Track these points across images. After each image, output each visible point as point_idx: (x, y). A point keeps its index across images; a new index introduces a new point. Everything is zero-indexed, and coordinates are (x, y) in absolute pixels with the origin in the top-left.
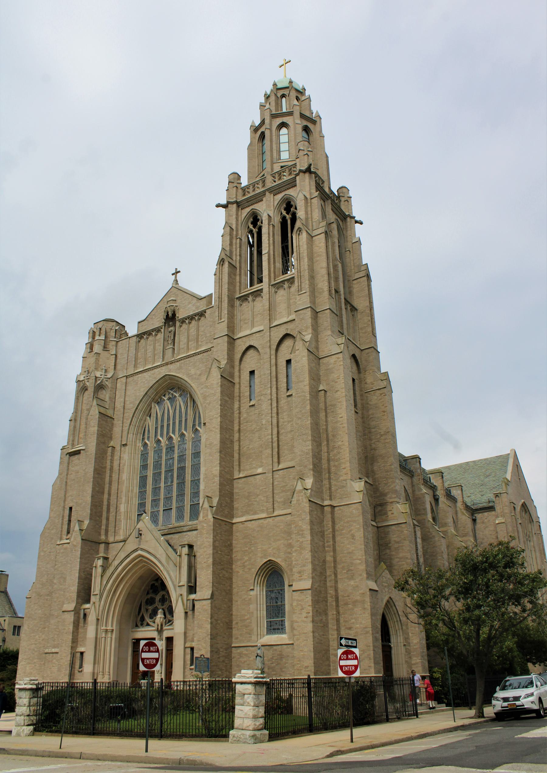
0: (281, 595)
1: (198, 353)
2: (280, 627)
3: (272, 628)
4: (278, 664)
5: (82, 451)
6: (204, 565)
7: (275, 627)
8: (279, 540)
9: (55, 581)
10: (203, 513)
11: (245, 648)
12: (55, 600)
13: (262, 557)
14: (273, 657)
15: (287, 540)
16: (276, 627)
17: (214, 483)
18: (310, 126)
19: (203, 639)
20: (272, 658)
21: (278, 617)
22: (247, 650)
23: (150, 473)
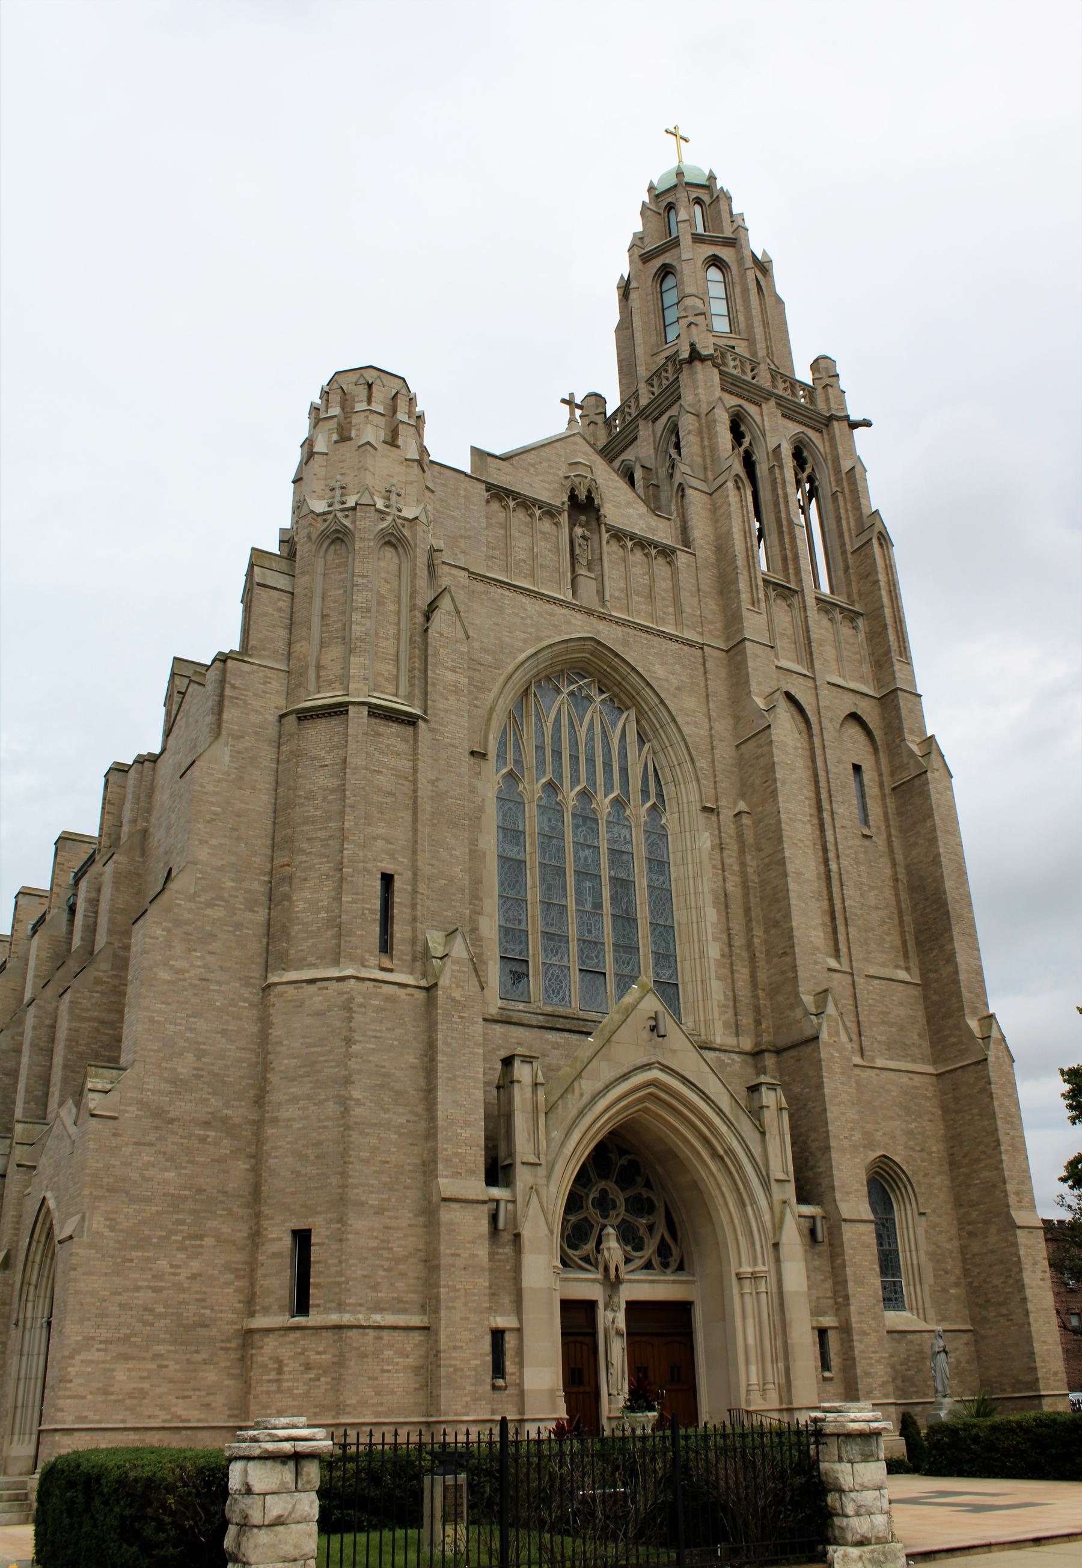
1: (671, 638)
4: (919, 1371)
5: (351, 708)
6: (846, 1143)
8: (892, 1118)
9: (356, 1094)
10: (829, 1026)
12: (365, 1155)
14: (909, 1356)
18: (725, 253)
19: (869, 1310)
20: (907, 1358)
23: (532, 855)
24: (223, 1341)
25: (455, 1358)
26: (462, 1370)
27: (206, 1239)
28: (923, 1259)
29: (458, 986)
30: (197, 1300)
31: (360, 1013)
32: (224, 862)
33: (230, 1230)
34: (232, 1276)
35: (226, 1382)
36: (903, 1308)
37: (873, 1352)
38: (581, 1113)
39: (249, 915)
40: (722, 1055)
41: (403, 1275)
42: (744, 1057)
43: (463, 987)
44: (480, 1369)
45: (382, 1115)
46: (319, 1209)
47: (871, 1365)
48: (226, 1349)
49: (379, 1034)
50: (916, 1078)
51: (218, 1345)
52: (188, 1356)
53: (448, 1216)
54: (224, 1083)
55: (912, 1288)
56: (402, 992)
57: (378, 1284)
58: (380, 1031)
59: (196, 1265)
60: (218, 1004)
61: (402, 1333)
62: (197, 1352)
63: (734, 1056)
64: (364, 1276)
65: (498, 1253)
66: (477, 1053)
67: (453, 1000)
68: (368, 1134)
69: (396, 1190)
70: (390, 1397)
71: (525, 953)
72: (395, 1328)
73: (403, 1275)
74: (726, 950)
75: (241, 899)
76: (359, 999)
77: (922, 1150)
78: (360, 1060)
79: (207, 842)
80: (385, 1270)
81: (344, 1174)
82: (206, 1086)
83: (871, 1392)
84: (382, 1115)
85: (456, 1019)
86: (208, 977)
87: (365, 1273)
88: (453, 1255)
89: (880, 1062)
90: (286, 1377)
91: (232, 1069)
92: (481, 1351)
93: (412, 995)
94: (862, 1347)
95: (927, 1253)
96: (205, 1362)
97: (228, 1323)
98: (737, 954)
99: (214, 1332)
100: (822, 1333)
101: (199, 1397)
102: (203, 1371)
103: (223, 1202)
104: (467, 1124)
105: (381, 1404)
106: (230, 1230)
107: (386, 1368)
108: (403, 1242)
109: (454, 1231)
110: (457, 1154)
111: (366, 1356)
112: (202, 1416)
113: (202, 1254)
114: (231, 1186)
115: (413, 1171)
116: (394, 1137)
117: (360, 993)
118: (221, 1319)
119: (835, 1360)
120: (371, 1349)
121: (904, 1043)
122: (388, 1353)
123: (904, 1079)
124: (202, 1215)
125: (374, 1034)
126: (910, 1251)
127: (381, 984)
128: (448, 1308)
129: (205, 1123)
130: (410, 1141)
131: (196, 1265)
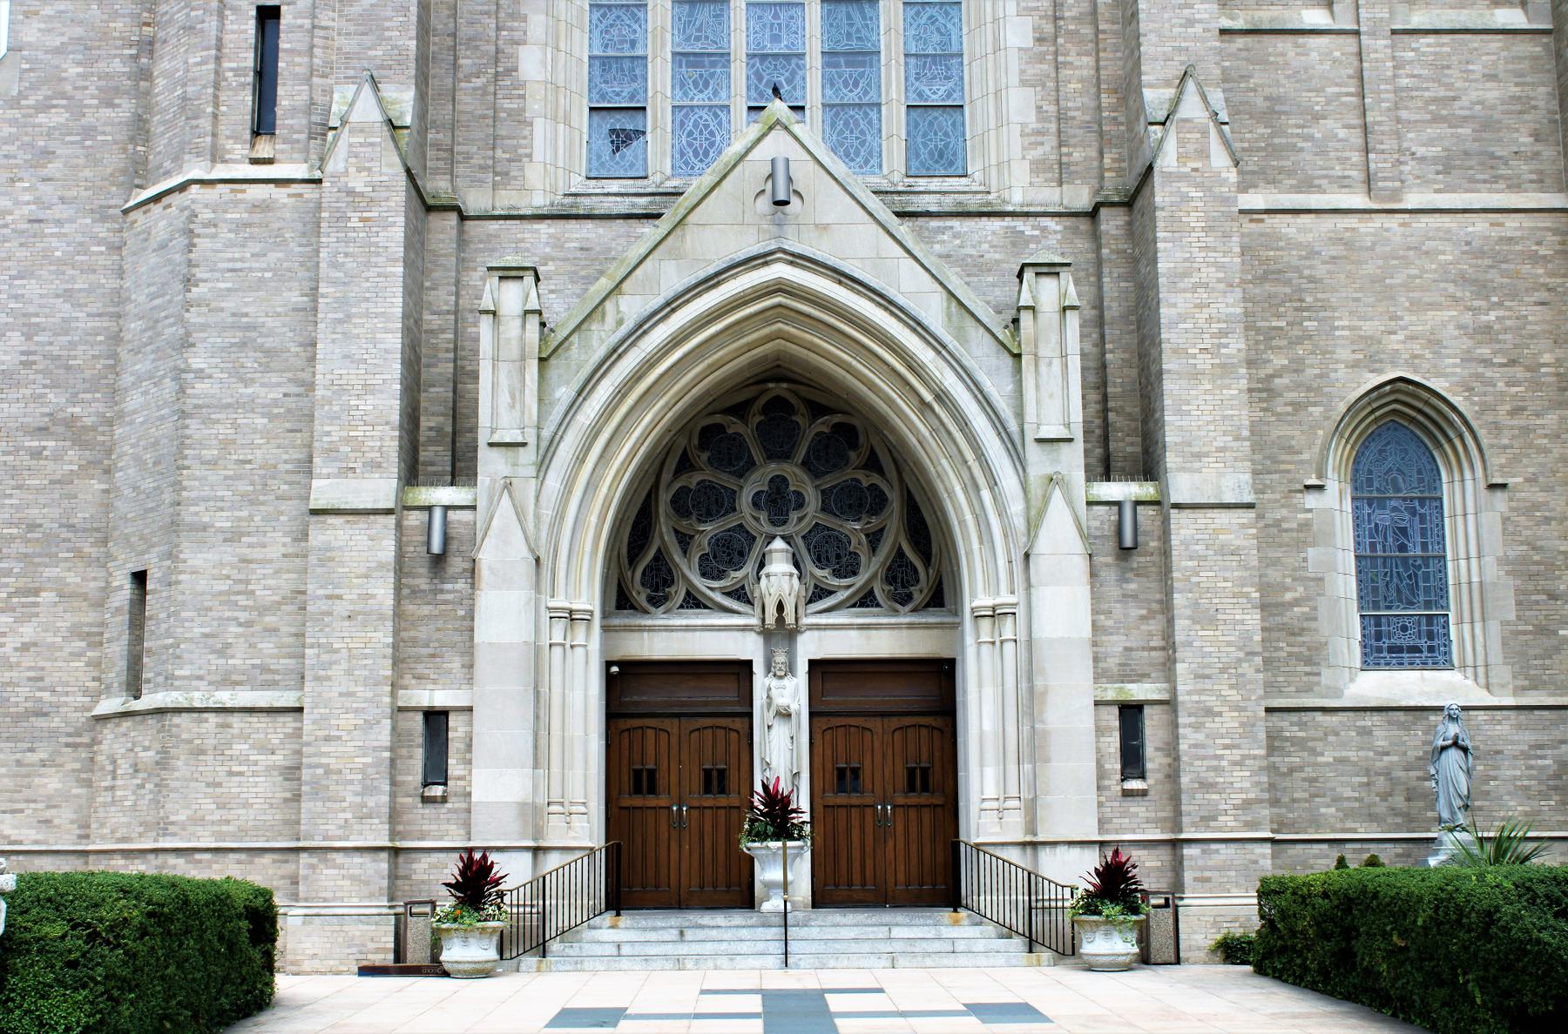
0: (1423, 519)
2: (1423, 643)
3: (1385, 643)
6: (1204, 362)
7: (1398, 643)
9: (197, 362)
11: (1294, 717)
12: (208, 454)
13: (1355, 365)
15: (1475, 310)
16: (1405, 641)
17: (1190, 23)
21: (1411, 604)
22: (1302, 725)
24: (69, 735)
25: (327, 755)
26: (340, 772)
27: (43, 594)
28: (1493, 571)
29: (359, 170)
30: (30, 679)
31: (207, 236)
32: (65, 39)
33: (78, 580)
34: (83, 644)
35: (75, 791)
36: (1448, 665)
37: (1226, 747)
38: (615, 354)
39: (107, 113)
40: (1019, 224)
41: (274, 630)
42: (1068, 222)
43: (369, 169)
44: (370, 770)
45: (243, 390)
46: (154, 540)
47: (1218, 770)
48: (75, 746)
49: (238, 265)
50: (1512, 222)
51: (63, 740)
52: (18, 756)
53: (321, 538)
54: (68, 368)
55: (1467, 627)
56: (281, 194)
57: (228, 645)
58: (242, 260)
59: (28, 631)
60: (58, 254)
61: (264, 718)
62: (31, 750)
63: (1050, 223)
64: (206, 636)
65: (442, 591)
66: (394, 275)
67: (351, 193)
68: (218, 421)
69: (262, 503)
71: (640, 97)
73: (274, 630)
74: (1049, 28)
75: (93, 90)
76: (206, 215)
77: (1512, 363)
78: (204, 309)
79: (37, 13)
80: (240, 625)
81: (178, 486)
82: (40, 376)
84: (243, 390)
85: (355, 223)
86: (41, 216)
87: (207, 630)
88: (329, 597)
89: (1412, 200)
90: (119, 783)
91: (79, 348)
93: (301, 195)
94: (1200, 737)
95: (1503, 561)
96: (43, 764)
97: (76, 710)
98: (1069, 32)
99: (56, 722)
100: (1131, 713)
101: (35, 810)
102: (40, 776)
103: (69, 540)
104: (368, 389)
105: (228, 822)
106: (78, 580)
107: (235, 769)
108: (271, 582)
109: (332, 559)
110: (347, 440)
111: (202, 752)
112: (40, 837)
113: (37, 615)
114: (79, 518)
115: (293, 472)
116: (261, 421)
117: (206, 206)
118: (66, 704)
119: (1154, 759)
120: (211, 742)
121: (1492, 156)
122: (239, 748)
123: (1479, 226)
124: (37, 560)
125: (230, 265)
126: (1468, 558)
127: (244, 186)
128: (317, 678)
129: (40, 429)
130: (288, 425)
131: (28, 631)
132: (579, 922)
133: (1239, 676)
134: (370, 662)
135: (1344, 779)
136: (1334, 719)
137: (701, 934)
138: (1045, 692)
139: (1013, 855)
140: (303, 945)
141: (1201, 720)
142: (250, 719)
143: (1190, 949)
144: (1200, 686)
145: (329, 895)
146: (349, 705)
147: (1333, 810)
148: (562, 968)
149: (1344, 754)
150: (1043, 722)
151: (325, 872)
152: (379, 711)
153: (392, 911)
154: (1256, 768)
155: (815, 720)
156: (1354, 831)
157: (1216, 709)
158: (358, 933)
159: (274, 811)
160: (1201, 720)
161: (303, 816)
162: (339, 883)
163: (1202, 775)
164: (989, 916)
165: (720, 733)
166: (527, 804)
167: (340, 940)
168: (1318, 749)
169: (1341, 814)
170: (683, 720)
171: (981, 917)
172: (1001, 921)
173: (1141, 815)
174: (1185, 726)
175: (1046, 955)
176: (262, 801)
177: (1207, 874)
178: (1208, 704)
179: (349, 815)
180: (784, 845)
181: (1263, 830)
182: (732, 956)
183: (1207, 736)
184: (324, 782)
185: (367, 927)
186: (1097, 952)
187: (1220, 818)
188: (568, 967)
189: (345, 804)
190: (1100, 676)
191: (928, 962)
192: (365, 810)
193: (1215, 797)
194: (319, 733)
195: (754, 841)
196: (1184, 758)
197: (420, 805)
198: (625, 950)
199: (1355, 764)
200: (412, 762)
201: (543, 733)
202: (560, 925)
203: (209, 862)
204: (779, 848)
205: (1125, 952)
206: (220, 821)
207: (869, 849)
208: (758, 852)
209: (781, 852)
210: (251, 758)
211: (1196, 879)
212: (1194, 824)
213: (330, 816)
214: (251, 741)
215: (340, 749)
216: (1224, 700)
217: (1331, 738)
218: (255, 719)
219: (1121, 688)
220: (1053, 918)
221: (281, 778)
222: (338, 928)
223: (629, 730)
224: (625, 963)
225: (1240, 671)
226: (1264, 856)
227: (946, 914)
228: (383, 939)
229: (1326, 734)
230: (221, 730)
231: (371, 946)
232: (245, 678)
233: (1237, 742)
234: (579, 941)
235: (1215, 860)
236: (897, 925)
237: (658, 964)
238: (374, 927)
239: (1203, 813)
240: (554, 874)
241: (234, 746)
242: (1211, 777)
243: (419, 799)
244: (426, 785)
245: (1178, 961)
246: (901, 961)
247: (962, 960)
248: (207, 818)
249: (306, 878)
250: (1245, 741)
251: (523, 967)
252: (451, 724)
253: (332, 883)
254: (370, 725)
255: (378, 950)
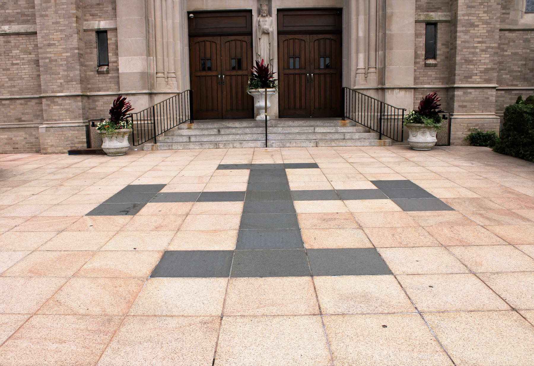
25: (49, 53)
26: (56, 61)
37: (479, 42)
44: (70, 59)
47: (474, 54)
70: (20, 81)
72: (18, 34)
83: (470, 77)
92: (71, 46)
94: (467, 37)
100: (431, 25)
105: (14, 86)
107: (15, 62)
119: (441, 50)
122: (15, 52)
128: (42, 16)
132: (172, 126)
133: (488, 6)
134: (65, 6)
135: (515, 62)
136: (514, 34)
137: (228, 131)
138: (392, 15)
139: (372, 94)
140: (47, 141)
141: (468, 29)
142: (18, 38)
143: (455, 139)
144: (469, 12)
145: (57, 118)
146: (57, 28)
147: (509, 76)
148: (163, 148)
149: (516, 51)
150: (390, 30)
151: (54, 107)
152: (71, 30)
153: (84, 125)
154: (492, 53)
155: (280, 36)
156: (517, 85)
157: (476, 23)
158: (70, 135)
159: (33, 81)
160: (468, 29)
161: (42, 82)
162: (60, 112)
163: (466, 56)
164: (360, 122)
165: (239, 42)
166: (145, 73)
167: (63, 138)
168: (505, 49)
169: (511, 78)
170: (222, 37)
171: (355, 123)
172: (366, 124)
173: (433, 76)
174: (460, 32)
175: (388, 141)
176: (28, 76)
177: (465, 104)
178: (472, 21)
179: (62, 81)
180: (266, 90)
181: (492, 83)
182: (241, 141)
183: (470, 37)
184: (50, 66)
185: (73, 132)
186: (418, 141)
187: (473, 77)
188: (166, 148)
189: (60, 76)
190: (418, 8)
191: (333, 144)
192: (69, 78)
193: (471, 67)
194: (45, 42)
195: (252, 89)
196: (459, 48)
197: (97, 75)
198: (193, 139)
199: (521, 55)
200: (92, 55)
201: (152, 40)
202: (163, 128)
203: (9, 105)
204: (263, 92)
205: (432, 141)
206: (11, 86)
207: (303, 92)
208: (255, 94)
209: (264, 93)
210: (21, 56)
211: (459, 106)
212: (460, 80)
213: (54, 81)
214: (20, 49)
215: (55, 50)
216: (480, 20)
217: (511, 44)
218: (21, 38)
219: (427, 15)
220: (392, 124)
221: (35, 66)
222: (61, 133)
223: (199, 42)
224: (192, 146)
225: (489, 4)
226: (492, 96)
227: (339, 122)
228: (82, 137)
229: (509, 42)
230: (6, 44)
231: (76, 140)
232: (14, 19)
233: (484, 40)
234: (173, 135)
235: (469, 97)
236: (318, 126)
237: (207, 146)
238: (77, 132)
239: (466, 75)
240: (159, 105)
241: (13, 52)
242: (471, 57)
243: (96, 73)
244: (100, 66)
245: (449, 144)
246: (321, 144)
247: (349, 143)
248: (5, 85)
249: (46, 110)
250: (488, 39)
251: (145, 148)
252: (109, 37)
253: (57, 113)
254: (68, 37)
255: (80, 143)
